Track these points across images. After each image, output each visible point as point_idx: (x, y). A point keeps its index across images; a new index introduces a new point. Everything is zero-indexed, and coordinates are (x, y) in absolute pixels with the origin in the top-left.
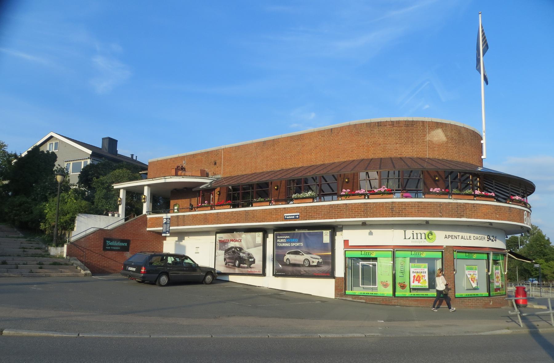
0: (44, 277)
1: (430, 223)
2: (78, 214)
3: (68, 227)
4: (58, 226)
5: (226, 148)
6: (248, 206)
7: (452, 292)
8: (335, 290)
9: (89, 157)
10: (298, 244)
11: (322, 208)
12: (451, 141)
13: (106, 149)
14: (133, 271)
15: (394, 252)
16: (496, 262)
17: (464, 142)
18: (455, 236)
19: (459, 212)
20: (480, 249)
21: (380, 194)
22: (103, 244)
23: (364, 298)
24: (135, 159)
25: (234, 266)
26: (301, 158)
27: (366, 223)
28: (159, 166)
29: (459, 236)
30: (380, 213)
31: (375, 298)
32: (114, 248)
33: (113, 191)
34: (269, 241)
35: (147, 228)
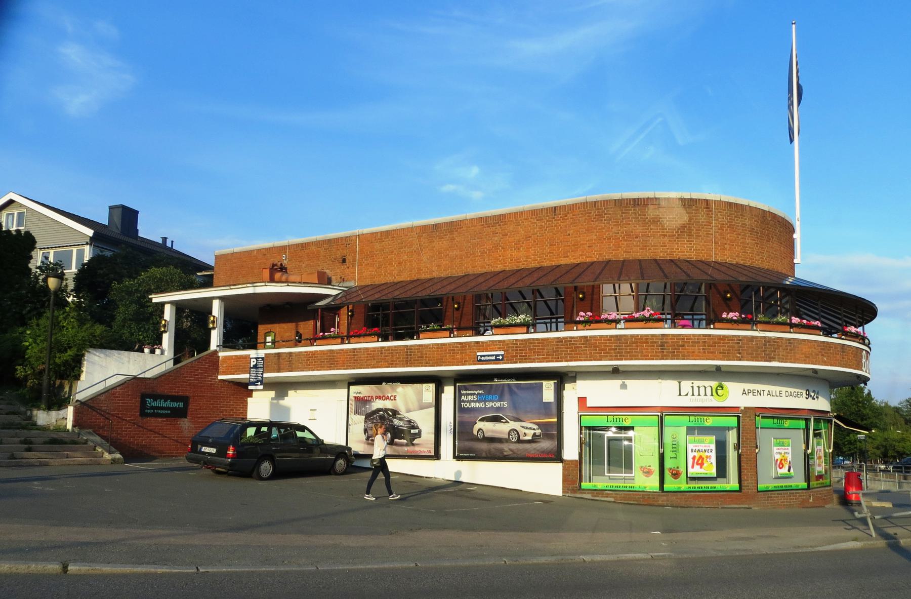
2: (87, 350)
3: (68, 373)
4: (50, 370)
5: (363, 234)
7: (752, 483)
8: (563, 481)
9: (88, 241)
10: (498, 404)
12: (750, 234)
14: (210, 454)
16: (817, 435)
17: (770, 235)
18: (758, 391)
19: (767, 353)
20: (794, 413)
21: (642, 321)
22: (139, 405)
23: (612, 494)
24: (170, 247)
26: (500, 256)
28: (235, 263)
29: (764, 391)
31: (630, 494)
32: (159, 412)
33: (150, 306)
34: (447, 399)
35: (218, 374)
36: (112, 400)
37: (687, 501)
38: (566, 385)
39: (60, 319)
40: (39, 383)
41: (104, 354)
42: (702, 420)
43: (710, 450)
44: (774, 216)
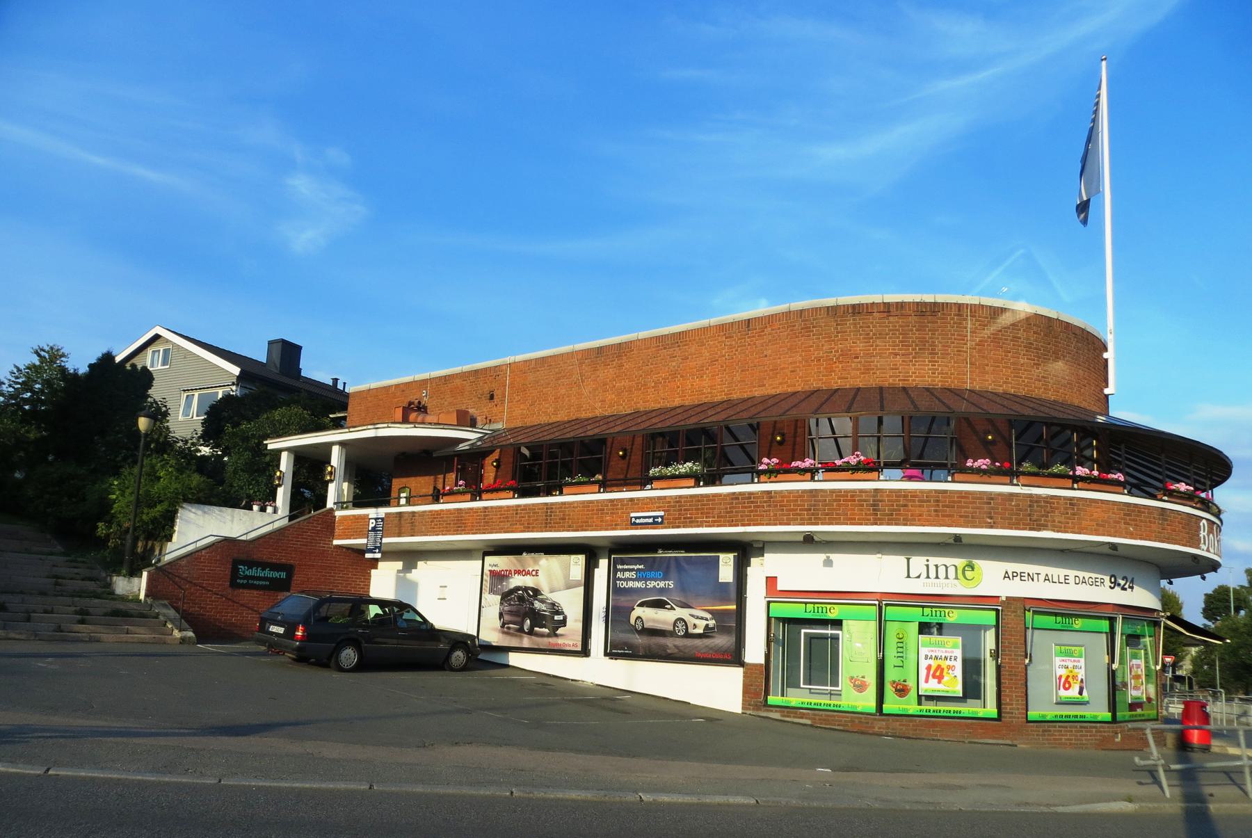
0: (86, 641)
1: (964, 541)
2: (181, 505)
4: (135, 529)
6: (549, 493)
7: (1018, 709)
9: (235, 381)
10: (662, 584)
11: (714, 500)
13: (276, 367)
14: (277, 635)
15: (880, 608)
18: (1029, 574)
19: (1035, 517)
20: (1088, 608)
21: (843, 470)
22: (230, 573)
24: (342, 389)
25: (521, 630)
27: (813, 537)
28: (370, 402)
29: (1038, 574)
30: (847, 514)
31: (834, 716)
32: (255, 582)
33: (267, 454)
36: (196, 565)
37: (916, 730)
38: (752, 559)
39: (157, 468)
40: (122, 544)
41: (202, 510)
42: (943, 614)
43: (953, 658)
44: (1068, 326)
